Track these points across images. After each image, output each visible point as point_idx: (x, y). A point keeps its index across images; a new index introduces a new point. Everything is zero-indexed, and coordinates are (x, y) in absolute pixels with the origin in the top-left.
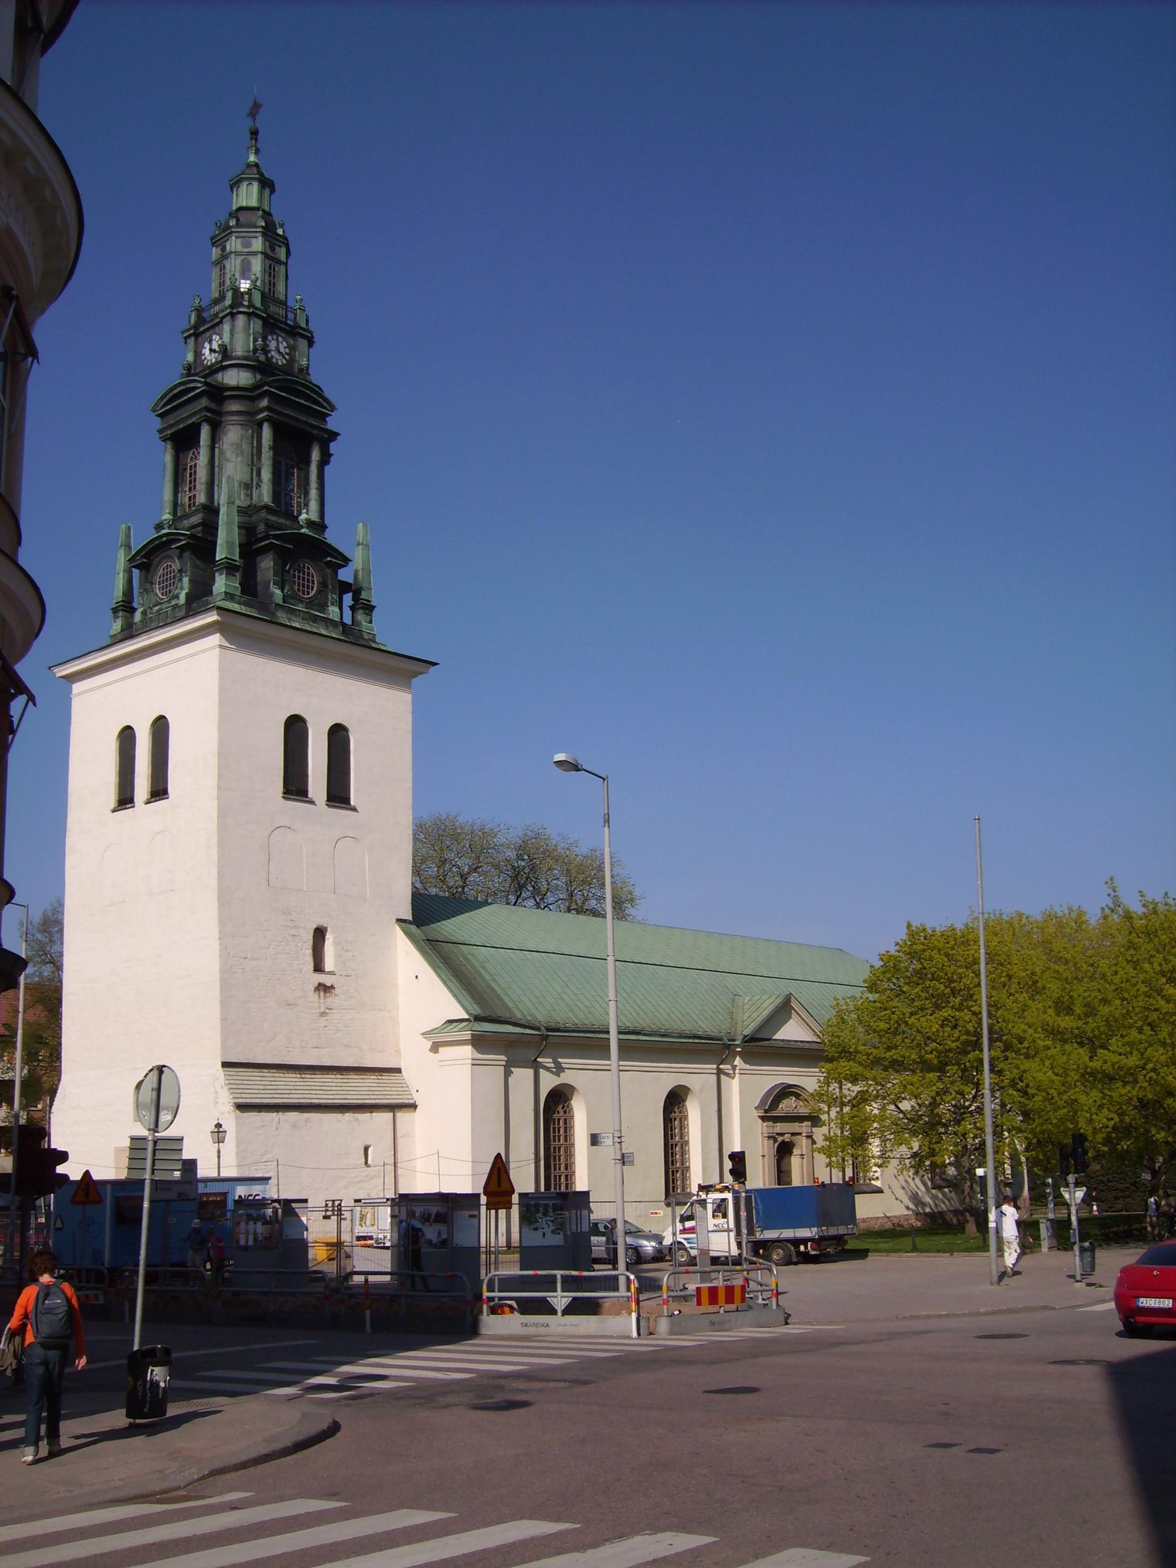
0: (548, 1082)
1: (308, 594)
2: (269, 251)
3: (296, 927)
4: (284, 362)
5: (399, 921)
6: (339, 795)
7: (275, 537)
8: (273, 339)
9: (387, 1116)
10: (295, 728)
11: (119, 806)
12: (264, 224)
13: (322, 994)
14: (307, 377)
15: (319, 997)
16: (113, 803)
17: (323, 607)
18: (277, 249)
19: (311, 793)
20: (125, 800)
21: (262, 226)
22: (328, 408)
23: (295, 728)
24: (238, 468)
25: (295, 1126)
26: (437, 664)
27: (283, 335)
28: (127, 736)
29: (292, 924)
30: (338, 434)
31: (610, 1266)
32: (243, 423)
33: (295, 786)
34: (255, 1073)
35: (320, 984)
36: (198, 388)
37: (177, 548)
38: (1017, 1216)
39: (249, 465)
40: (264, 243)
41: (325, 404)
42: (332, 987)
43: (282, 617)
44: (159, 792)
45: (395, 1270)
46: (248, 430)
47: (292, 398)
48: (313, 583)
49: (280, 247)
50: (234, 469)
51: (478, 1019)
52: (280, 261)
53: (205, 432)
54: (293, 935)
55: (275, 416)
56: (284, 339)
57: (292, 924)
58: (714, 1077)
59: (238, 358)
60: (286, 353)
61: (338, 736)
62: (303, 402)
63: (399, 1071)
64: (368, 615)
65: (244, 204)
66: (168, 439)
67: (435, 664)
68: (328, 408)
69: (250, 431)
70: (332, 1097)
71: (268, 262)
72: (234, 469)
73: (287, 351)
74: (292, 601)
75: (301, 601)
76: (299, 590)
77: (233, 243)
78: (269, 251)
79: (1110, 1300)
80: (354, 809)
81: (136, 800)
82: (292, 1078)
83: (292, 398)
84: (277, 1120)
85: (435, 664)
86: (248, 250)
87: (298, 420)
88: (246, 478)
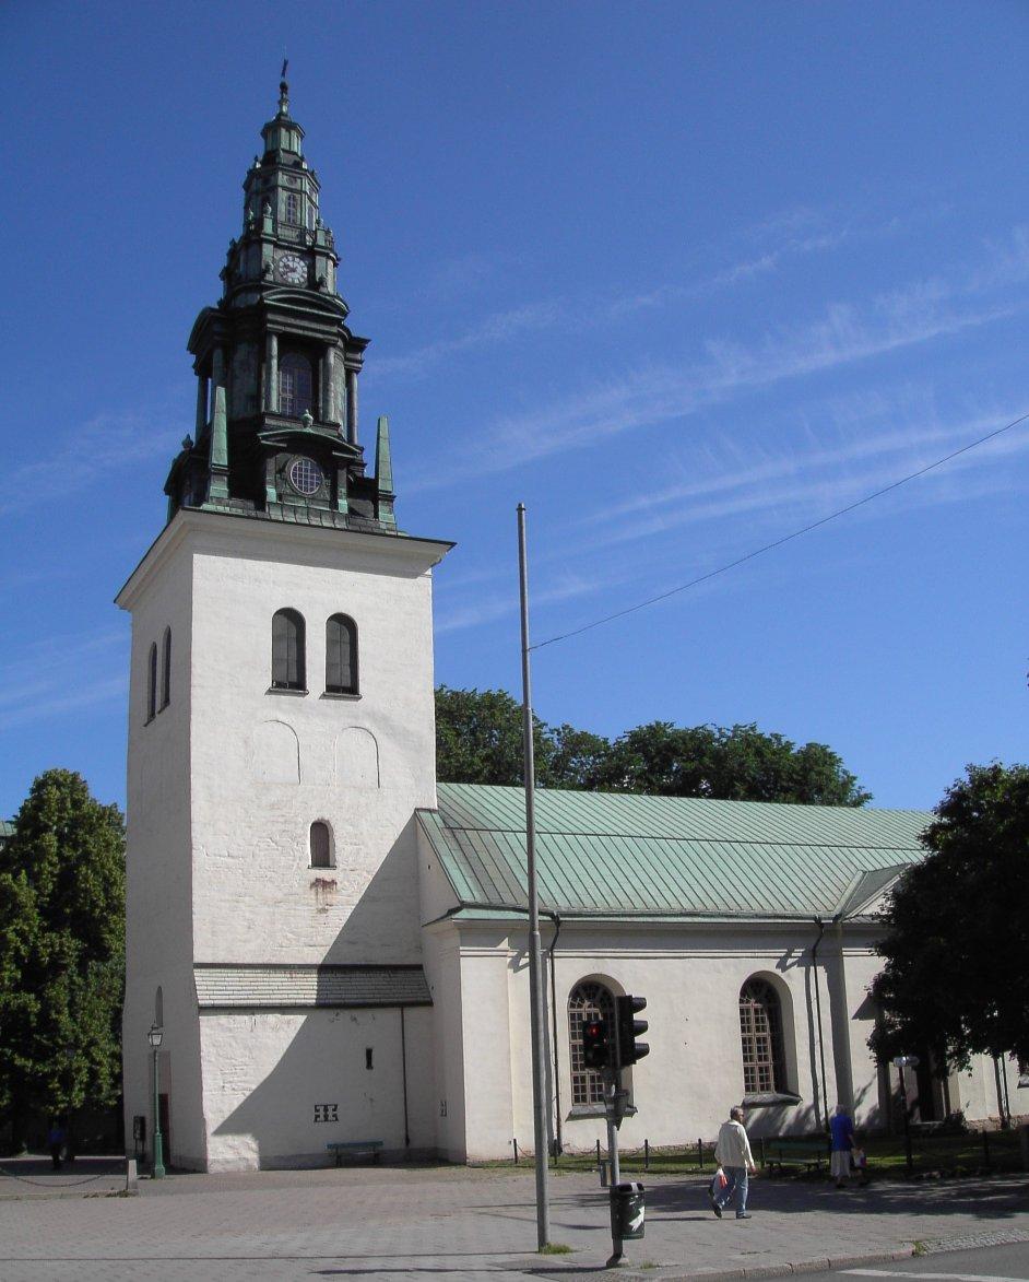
4: (302, 280)
6: (344, 686)
7: (265, 438)
9: (396, 1012)
10: (290, 623)
13: (320, 890)
15: (317, 894)
30: (367, 341)
33: (290, 680)
34: (234, 973)
35: (317, 880)
38: (26, 1152)
42: (333, 882)
43: (275, 514)
44: (167, 701)
45: (1013, 1125)
47: (289, 306)
48: (294, 475)
61: (343, 627)
63: (419, 968)
69: (257, 346)
74: (291, 499)
77: (282, 207)
82: (279, 978)
83: (289, 306)
84: (249, 1024)
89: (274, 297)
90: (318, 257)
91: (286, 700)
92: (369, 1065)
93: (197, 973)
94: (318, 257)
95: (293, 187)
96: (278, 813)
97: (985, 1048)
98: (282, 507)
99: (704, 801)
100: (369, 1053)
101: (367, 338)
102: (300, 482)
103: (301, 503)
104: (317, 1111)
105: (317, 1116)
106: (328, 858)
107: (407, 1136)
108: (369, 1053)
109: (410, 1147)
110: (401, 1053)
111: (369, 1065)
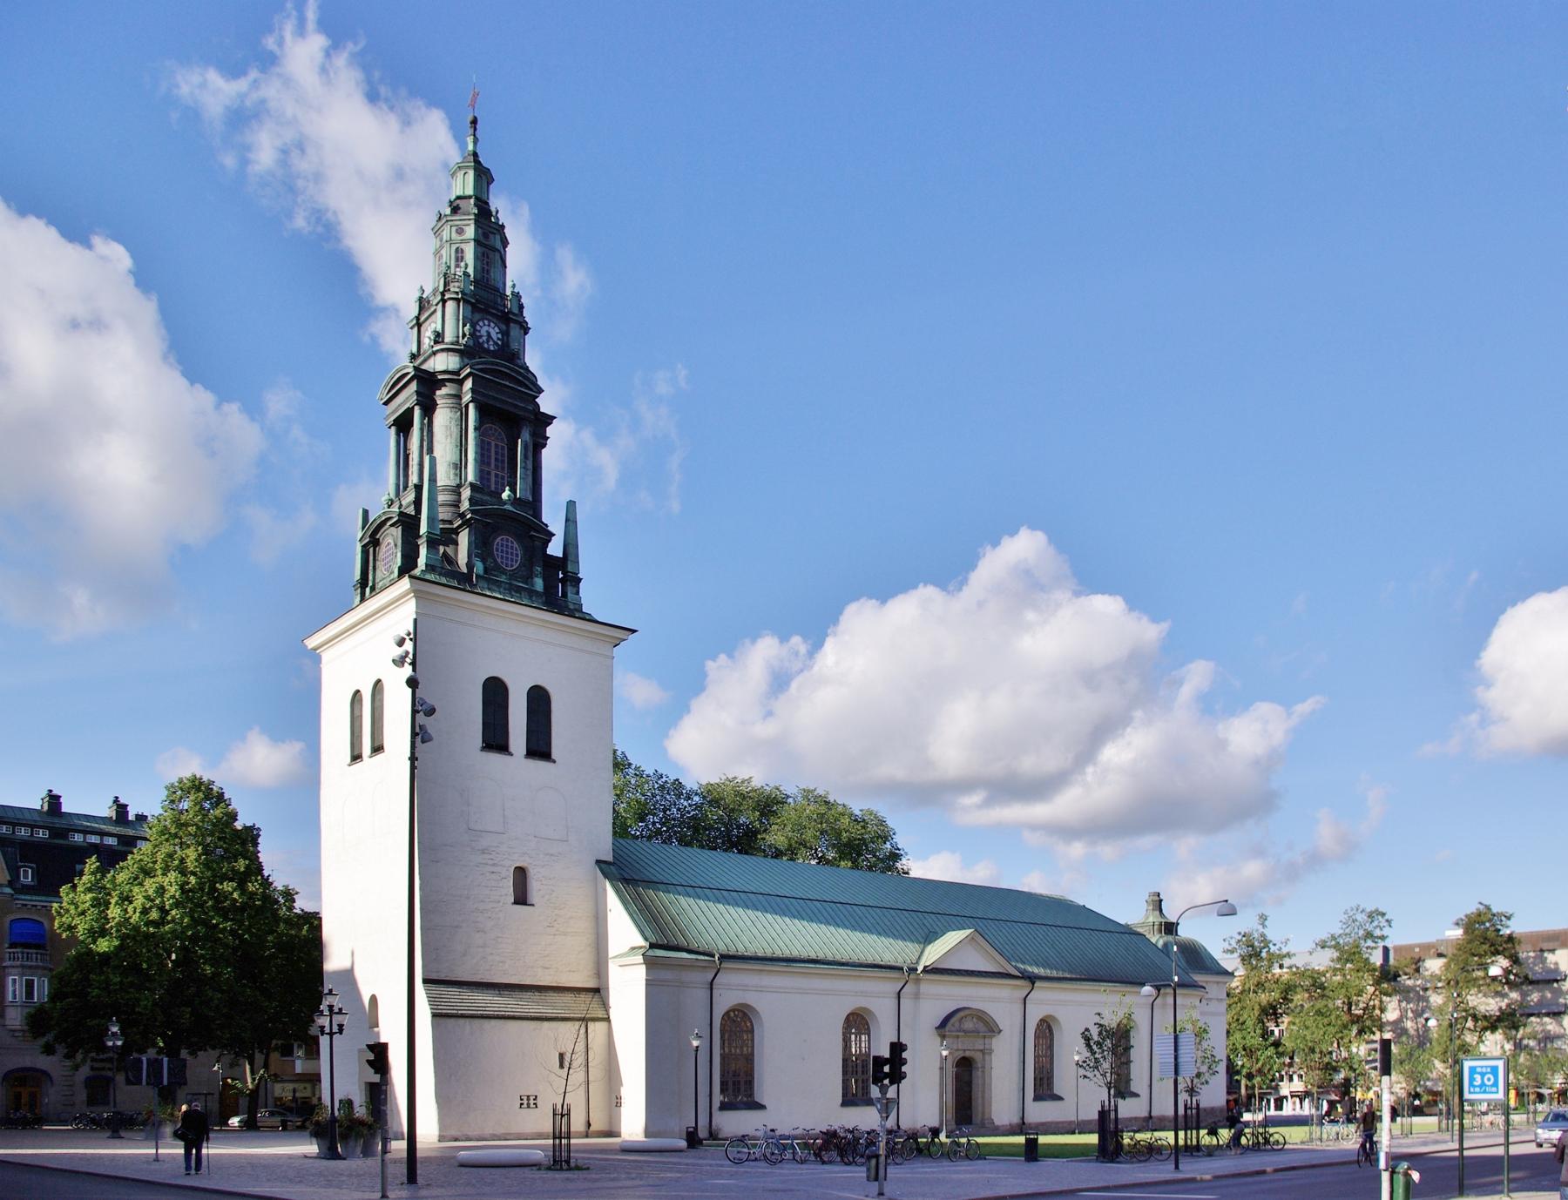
0: (725, 1001)
1: (512, 566)
2: (482, 239)
3: (494, 865)
5: (598, 862)
6: (539, 748)
8: (485, 325)
11: (352, 761)
12: (476, 212)
14: (519, 361)
16: (348, 759)
17: (528, 578)
18: (491, 236)
19: (512, 748)
20: (356, 757)
21: (475, 214)
22: (535, 390)
23: (495, 692)
24: (448, 448)
25: (534, 1030)
26: (636, 631)
27: (495, 321)
28: (357, 696)
29: (491, 862)
31: (1253, 1100)
32: (451, 405)
36: (408, 373)
37: (391, 525)
39: (457, 446)
40: (476, 230)
41: (531, 386)
44: (377, 749)
46: (456, 412)
49: (495, 234)
50: (444, 449)
51: (652, 946)
52: (494, 248)
53: (417, 412)
54: (493, 872)
55: (479, 398)
56: (496, 325)
57: (491, 862)
58: (893, 1002)
59: (447, 344)
60: (498, 339)
61: (539, 700)
62: (507, 383)
64: (574, 586)
65: (461, 194)
66: (392, 425)
67: (634, 631)
68: (535, 390)
70: (527, 1010)
71: (481, 249)
72: (444, 449)
73: (500, 336)
75: (504, 572)
76: (502, 562)
78: (482, 239)
79: (1500, 1136)
80: (554, 762)
81: (363, 755)
82: (518, 1011)
83: (519, 388)
85: (634, 631)
86: (462, 238)
87: (516, 406)
88: (455, 458)
89: (476, 367)
90: (512, 325)
91: (495, 758)
92: (521, 874)
93: (896, 1085)
94: (512, 325)
95: (486, 243)
96: (486, 856)
97: (202, 1144)
98: (488, 580)
99: (706, 852)
100: (521, 899)
101: (554, 532)
102: (502, 557)
103: (503, 578)
104: (522, 1100)
105: (522, 1104)
106: (526, 898)
107: (589, 1121)
108: (521, 899)
109: (591, 1128)
110: (897, 1027)
111: (521, 874)
